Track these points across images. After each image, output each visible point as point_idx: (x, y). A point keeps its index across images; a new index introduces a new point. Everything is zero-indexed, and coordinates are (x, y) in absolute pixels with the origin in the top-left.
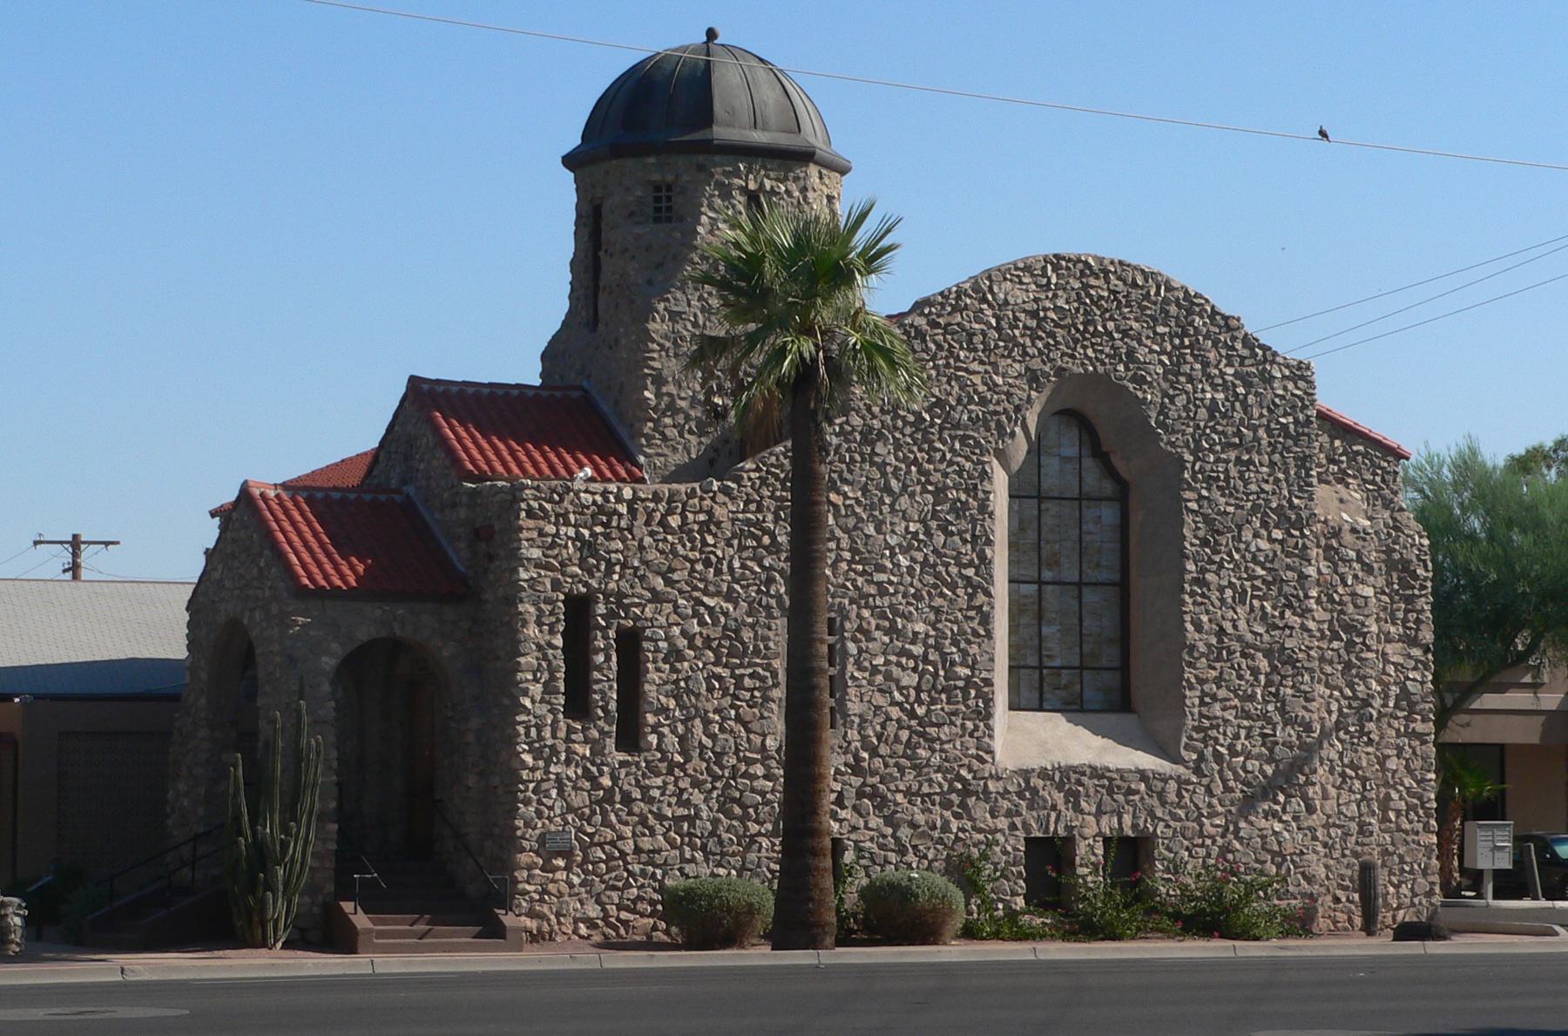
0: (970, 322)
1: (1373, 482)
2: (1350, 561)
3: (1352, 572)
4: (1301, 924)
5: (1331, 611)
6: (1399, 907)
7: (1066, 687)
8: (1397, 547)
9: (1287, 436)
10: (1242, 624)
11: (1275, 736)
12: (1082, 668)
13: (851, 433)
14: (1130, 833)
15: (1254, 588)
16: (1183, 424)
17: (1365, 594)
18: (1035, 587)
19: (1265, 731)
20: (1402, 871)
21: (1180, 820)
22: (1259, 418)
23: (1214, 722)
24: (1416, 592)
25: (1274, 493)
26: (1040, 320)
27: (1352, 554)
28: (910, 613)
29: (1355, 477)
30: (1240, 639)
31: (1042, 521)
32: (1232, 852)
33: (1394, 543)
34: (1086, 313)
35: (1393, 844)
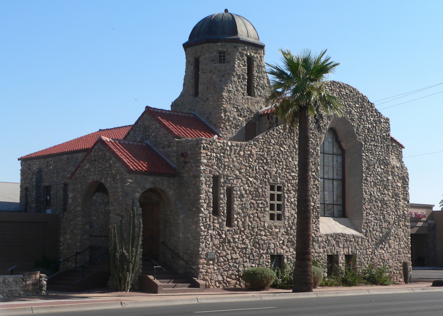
1: (397, 154)
7: (330, 210)
21: (362, 250)
30: (375, 197)
31: (325, 160)
32: (373, 259)
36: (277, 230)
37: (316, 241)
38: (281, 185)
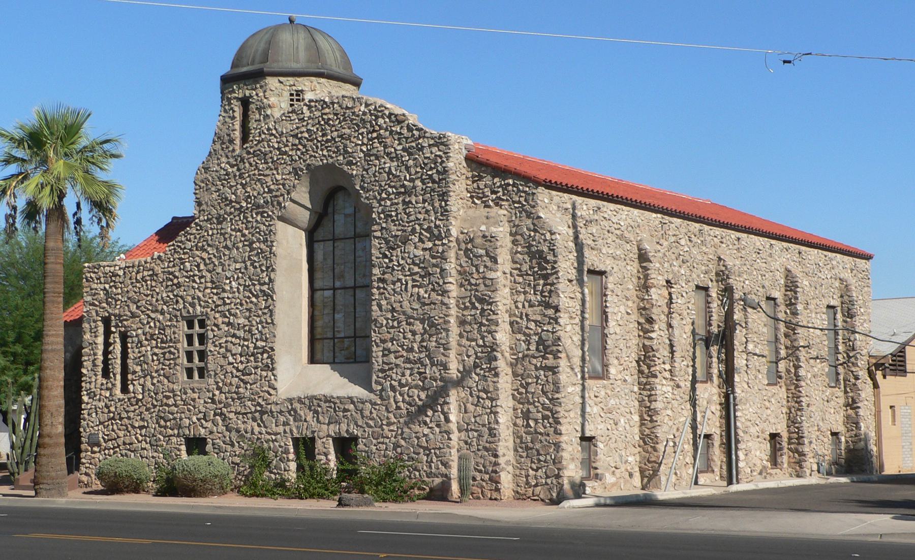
0: (265, 148)
1: (519, 202)
2: (481, 256)
3: (483, 264)
4: (440, 494)
5: (470, 290)
6: (536, 485)
7: (347, 349)
8: (534, 243)
9: (434, 182)
10: (406, 304)
11: (425, 373)
12: (355, 337)
13: (211, 219)
14: (346, 435)
15: (414, 280)
16: (373, 185)
17: (491, 277)
18: (332, 292)
19: (421, 370)
20: (539, 461)
21: (371, 427)
22: (415, 174)
23: (390, 366)
24: (549, 271)
25: (424, 220)
26: (300, 139)
27: (482, 252)
28: (236, 313)
29: (507, 200)
30: (404, 313)
31: (336, 253)
32: (399, 447)
33: (533, 240)
34: (323, 130)
35: (532, 442)
36: (196, 396)
37: (267, 412)
38: (204, 317)
